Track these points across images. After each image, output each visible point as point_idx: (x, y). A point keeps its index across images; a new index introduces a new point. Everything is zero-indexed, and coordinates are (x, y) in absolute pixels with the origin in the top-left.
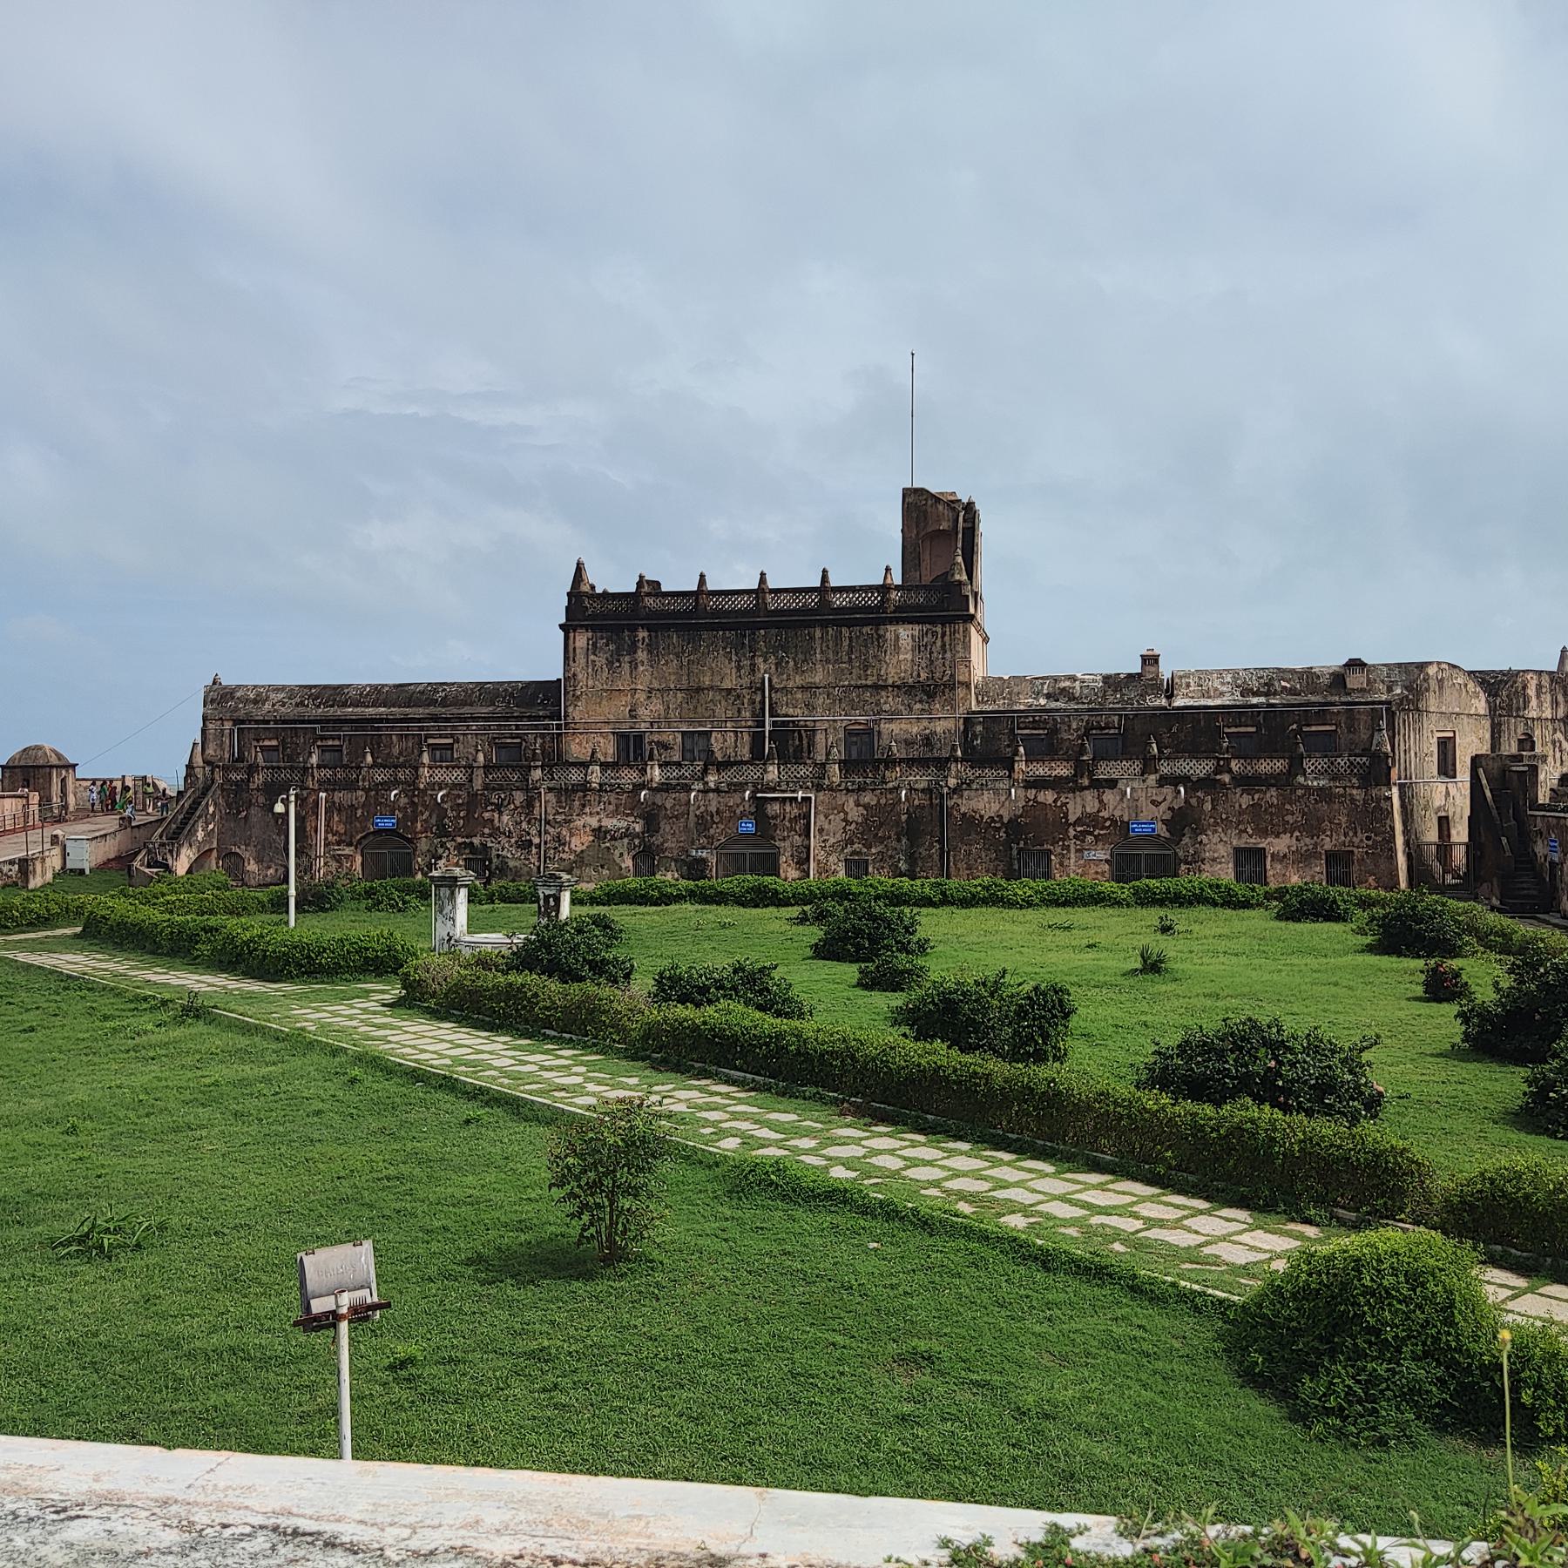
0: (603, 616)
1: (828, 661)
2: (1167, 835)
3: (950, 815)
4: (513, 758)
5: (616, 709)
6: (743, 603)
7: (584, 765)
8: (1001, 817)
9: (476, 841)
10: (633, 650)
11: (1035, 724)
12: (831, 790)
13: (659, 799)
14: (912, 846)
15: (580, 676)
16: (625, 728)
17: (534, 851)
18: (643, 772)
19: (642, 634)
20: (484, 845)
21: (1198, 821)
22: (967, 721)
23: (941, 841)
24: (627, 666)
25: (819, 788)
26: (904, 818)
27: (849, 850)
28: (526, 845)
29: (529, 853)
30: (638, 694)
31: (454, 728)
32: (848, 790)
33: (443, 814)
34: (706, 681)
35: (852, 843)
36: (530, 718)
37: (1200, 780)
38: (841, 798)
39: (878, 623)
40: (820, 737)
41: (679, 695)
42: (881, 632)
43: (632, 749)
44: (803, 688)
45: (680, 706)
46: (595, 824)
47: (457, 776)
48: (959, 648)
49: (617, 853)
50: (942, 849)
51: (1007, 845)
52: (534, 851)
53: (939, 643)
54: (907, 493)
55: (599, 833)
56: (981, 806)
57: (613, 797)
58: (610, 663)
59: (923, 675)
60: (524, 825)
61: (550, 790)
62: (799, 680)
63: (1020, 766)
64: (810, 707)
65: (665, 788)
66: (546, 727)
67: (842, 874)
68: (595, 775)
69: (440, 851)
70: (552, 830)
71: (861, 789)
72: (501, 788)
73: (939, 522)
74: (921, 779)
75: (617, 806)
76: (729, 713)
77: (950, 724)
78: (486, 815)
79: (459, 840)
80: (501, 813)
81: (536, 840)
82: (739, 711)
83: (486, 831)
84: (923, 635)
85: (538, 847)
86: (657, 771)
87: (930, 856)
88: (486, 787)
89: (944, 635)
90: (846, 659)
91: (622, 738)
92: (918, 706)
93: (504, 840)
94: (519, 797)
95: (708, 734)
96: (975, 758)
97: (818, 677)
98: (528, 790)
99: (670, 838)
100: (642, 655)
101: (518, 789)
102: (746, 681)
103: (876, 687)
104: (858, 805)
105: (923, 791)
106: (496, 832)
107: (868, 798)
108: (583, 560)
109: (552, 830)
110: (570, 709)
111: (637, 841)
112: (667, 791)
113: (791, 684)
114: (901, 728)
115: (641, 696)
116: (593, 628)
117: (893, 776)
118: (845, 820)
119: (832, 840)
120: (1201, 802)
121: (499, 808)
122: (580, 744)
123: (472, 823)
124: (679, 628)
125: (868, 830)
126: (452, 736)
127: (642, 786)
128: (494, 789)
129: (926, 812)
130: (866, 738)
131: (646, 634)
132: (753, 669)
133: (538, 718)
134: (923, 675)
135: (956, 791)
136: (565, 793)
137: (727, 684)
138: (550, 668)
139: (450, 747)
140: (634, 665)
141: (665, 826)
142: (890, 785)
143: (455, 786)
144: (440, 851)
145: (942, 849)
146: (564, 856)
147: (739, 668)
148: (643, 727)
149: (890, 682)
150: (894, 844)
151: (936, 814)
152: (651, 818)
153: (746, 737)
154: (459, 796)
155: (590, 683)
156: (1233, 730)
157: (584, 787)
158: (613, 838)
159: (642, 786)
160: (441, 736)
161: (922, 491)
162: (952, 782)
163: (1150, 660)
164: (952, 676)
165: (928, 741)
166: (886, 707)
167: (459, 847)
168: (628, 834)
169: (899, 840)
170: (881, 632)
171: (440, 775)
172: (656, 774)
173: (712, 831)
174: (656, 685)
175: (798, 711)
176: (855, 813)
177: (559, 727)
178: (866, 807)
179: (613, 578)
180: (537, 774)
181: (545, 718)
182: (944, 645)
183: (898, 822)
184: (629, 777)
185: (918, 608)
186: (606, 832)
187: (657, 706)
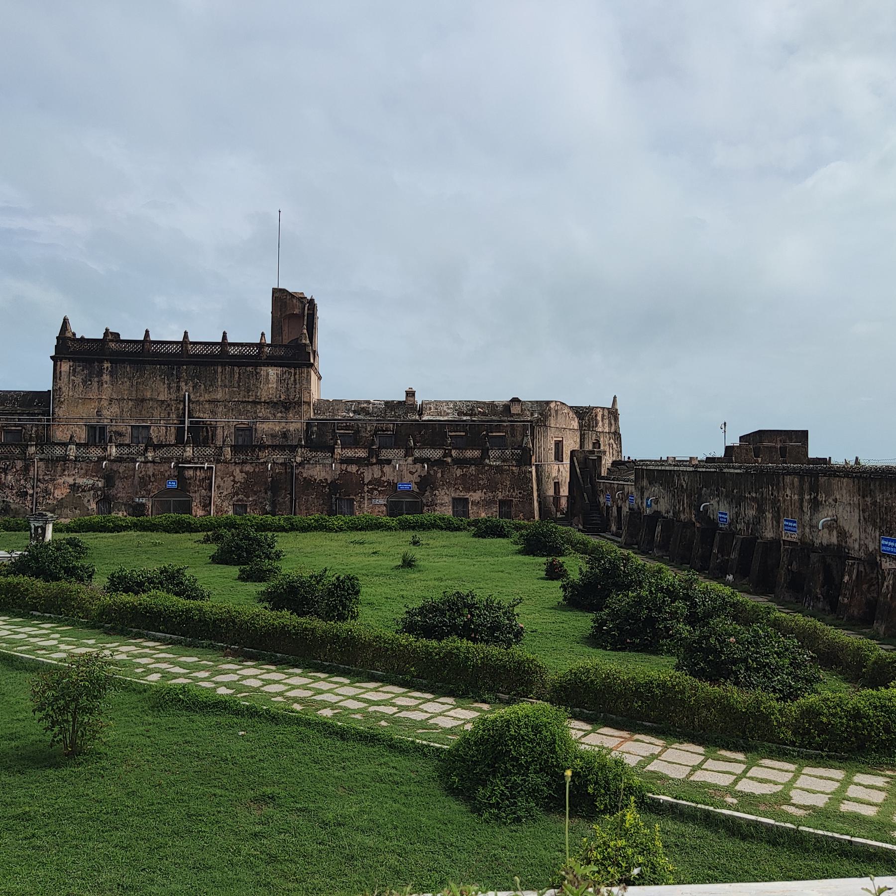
1: (225, 386)
5: (87, 411)
6: (173, 349)
7: (65, 445)
10: (100, 374)
11: (347, 428)
13: (115, 466)
15: (64, 389)
16: (93, 422)
17: (29, 498)
18: (105, 449)
23: (291, 494)
24: (96, 384)
25: (218, 461)
26: (269, 480)
27: (235, 498)
30: (104, 401)
32: (236, 463)
36: (28, 414)
37: (435, 460)
38: (231, 468)
39: (256, 365)
40: (219, 431)
41: (130, 403)
43: (98, 435)
45: (131, 409)
49: (86, 500)
50: (292, 498)
53: (292, 379)
54: (275, 291)
55: (74, 487)
56: (315, 473)
57: (84, 465)
58: (84, 382)
59: (283, 397)
60: (22, 482)
61: (41, 460)
63: (338, 451)
65: (119, 460)
67: (231, 513)
68: (72, 451)
71: (244, 462)
72: (7, 458)
73: (293, 309)
74: (280, 457)
77: (299, 426)
80: (6, 474)
81: (31, 492)
84: (284, 373)
85: (32, 495)
86: (114, 450)
91: (91, 429)
92: (280, 415)
93: (7, 491)
94: (19, 464)
96: (312, 446)
97: (219, 396)
98: (25, 460)
99: (121, 490)
100: (106, 377)
101: (19, 459)
102: (173, 396)
104: (241, 472)
105: (281, 464)
107: (248, 468)
109: (41, 485)
110: (56, 410)
111: (99, 493)
112: (120, 462)
113: (202, 399)
114: (268, 426)
115: (105, 403)
117: (263, 455)
118: (234, 481)
119: (225, 493)
120: (436, 472)
122: (62, 431)
127: (104, 459)
130: (247, 433)
131: (109, 365)
132: (178, 389)
133: (34, 414)
134: (283, 397)
135: (300, 464)
136: (51, 462)
137: (161, 398)
138: (45, 384)
140: (101, 383)
141: (119, 484)
142: (262, 460)
147: (169, 388)
148: (106, 422)
149: (263, 400)
152: (109, 479)
153: (173, 429)
155: (71, 394)
158: (83, 491)
162: (299, 459)
163: (410, 394)
165: (285, 435)
166: (260, 415)
168: (93, 488)
169: (266, 493)
170: (258, 371)
173: (149, 487)
174: (115, 396)
176: (240, 477)
177: (48, 420)
178: (247, 473)
179: (88, 328)
180: (32, 450)
182: (295, 380)
184: (95, 453)
186: (79, 487)
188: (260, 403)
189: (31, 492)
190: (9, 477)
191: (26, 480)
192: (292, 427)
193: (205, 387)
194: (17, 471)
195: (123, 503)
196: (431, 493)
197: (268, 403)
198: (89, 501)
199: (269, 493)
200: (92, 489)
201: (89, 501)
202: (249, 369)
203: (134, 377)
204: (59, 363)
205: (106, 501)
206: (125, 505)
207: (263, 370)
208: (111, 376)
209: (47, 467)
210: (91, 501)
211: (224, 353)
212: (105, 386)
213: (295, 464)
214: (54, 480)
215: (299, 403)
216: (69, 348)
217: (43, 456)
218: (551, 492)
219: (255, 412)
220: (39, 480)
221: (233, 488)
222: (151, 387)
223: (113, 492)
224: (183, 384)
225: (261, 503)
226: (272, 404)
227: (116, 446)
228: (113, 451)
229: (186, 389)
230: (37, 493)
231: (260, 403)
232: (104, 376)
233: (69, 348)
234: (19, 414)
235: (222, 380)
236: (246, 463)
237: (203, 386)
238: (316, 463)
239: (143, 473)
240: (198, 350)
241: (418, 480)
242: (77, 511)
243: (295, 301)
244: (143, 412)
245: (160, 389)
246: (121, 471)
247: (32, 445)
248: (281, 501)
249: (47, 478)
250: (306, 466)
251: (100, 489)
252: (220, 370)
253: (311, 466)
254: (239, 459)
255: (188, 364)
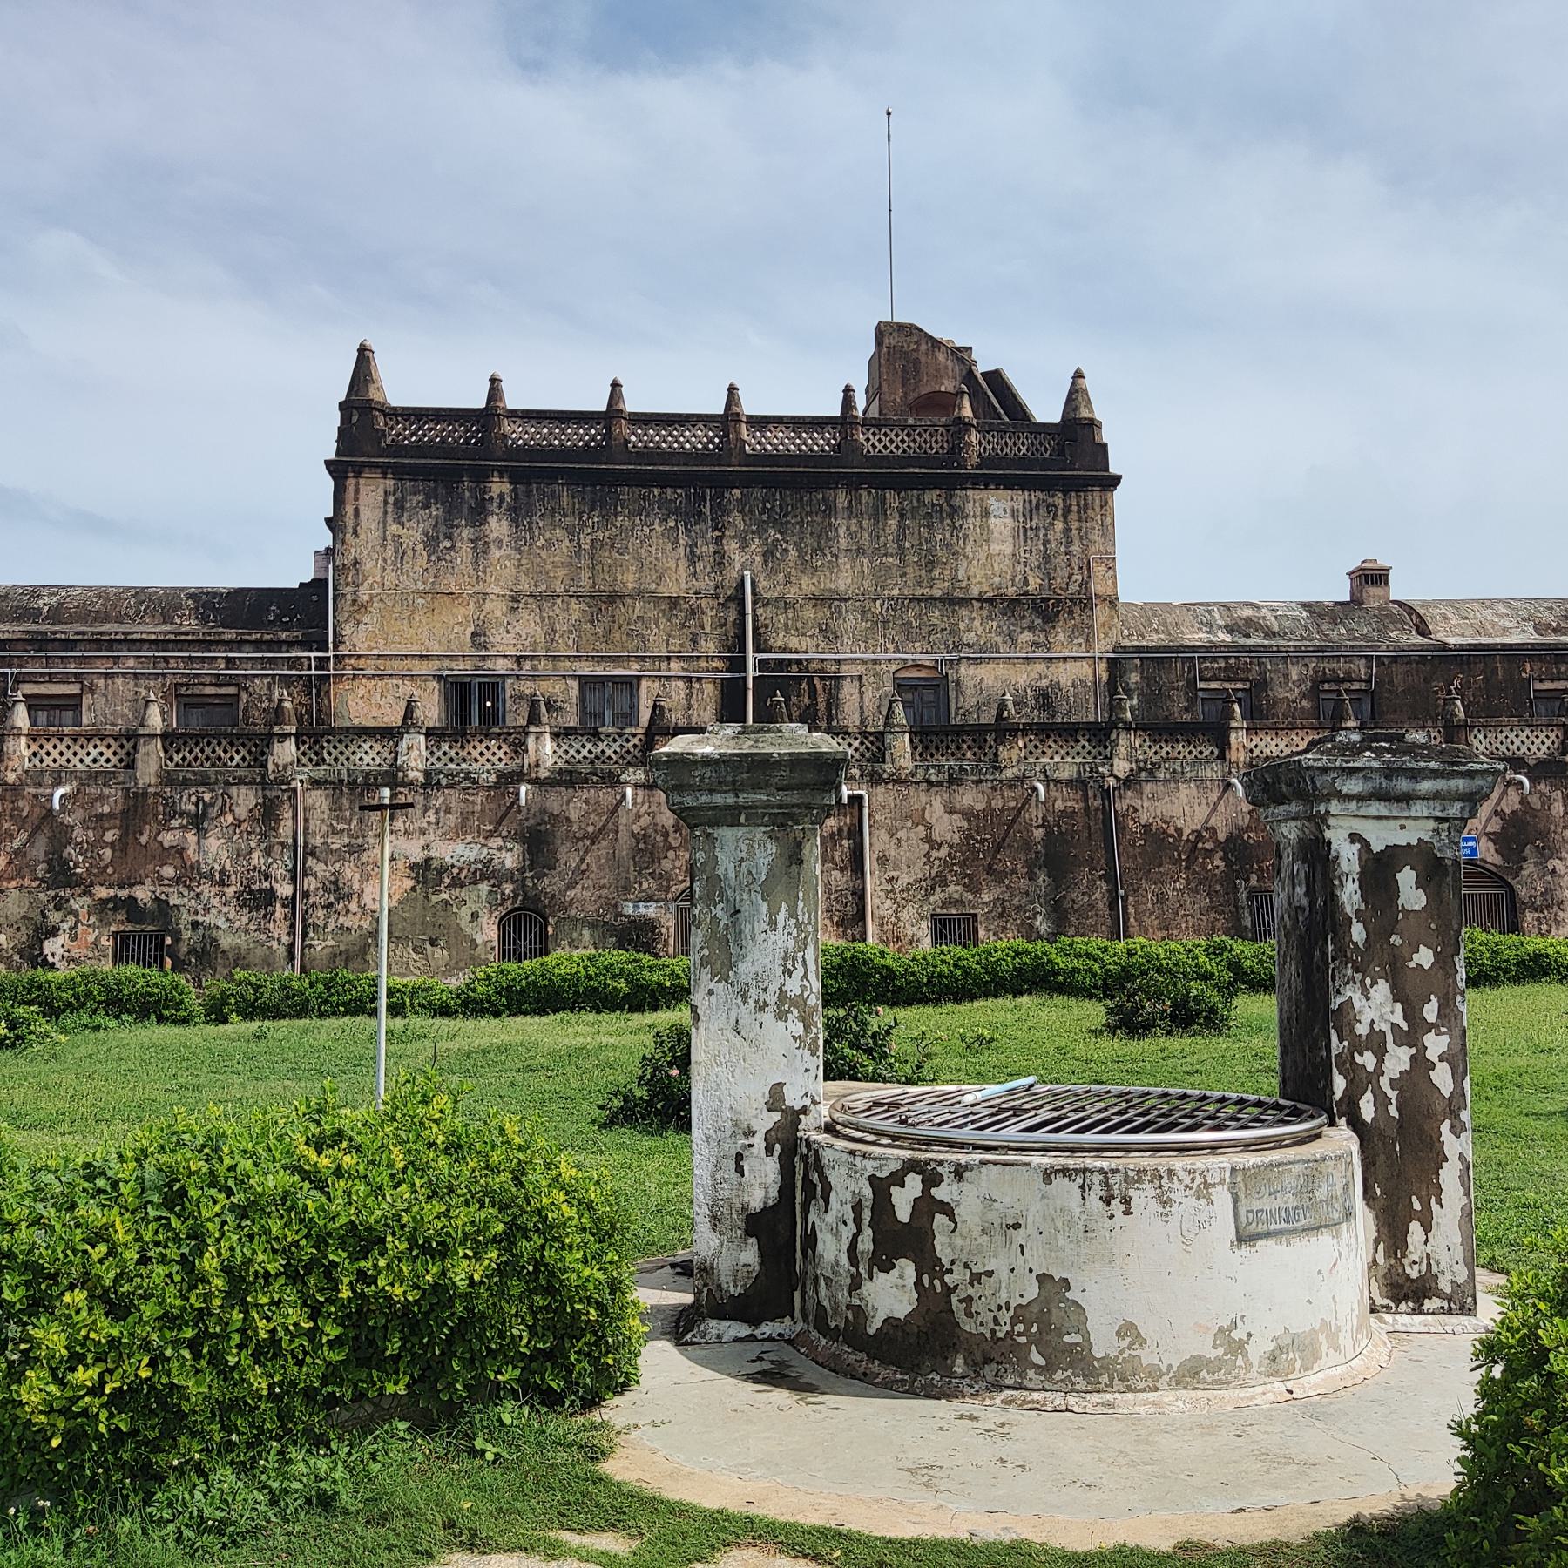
0: (419, 450)
1: (860, 551)
2: (1497, 860)
3: (1122, 828)
4: (216, 727)
5: (442, 634)
6: (695, 439)
7: (388, 734)
8: (1213, 830)
9: (143, 894)
10: (479, 513)
11: (1230, 674)
12: (898, 781)
13: (555, 801)
14: (1056, 889)
15: (368, 565)
16: (462, 669)
17: (279, 912)
18: (519, 748)
19: (499, 487)
20: (161, 904)
21: (1544, 835)
22: (1115, 665)
23: (1110, 878)
24: (465, 550)
25: (876, 779)
26: (1038, 834)
27: (938, 896)
28: (258, 900)
29: (268, 916)
30: (485, 600)
31: (84, 661)
32: (930, 783)
33: (61, 836)
34: (628, 580)
35: (945, 884)
36: (258, 645)
37: (1540, 763)
38: (919, 798)
39: (952, 484)
40: (848, 690)
41: (574, 605)
42: (957, 502)
43: (473, 705)
44: (818, 600)
45: (577, 626)
46: (417, 855)
47: (100, 755)
48: (1095, 535)
49: (465, 913)
50: (1113, 891)
51: (1229, 879)
52: (279, 912)
53: (1059, 526)
54: (881, 332)
55: (426, 873)
56: (1176, 810)
57: (454, 798)
58: (431, 541)
59: (1034, 582)
60: (257, 859)
61: (316, 783)
62: (807, 585)
63: (1238, 739)
64: (829, 634)
65: (567, 779)
66: (294, 663)
67: (926, 945)
68: (416, 755)
69: (55, 917)
70: (319, 868)
71: (954, 780)
72: (203, 781)
73: (938, 378)
74: (1065, 763)
75: (465, 817)
76: (676, 644)
77: (1084, 670)
78: (168, 838)
79: (102, 892)
80: (201, 833)
81: (285, 890)
82: (694, 640)
83: (168, 871)
84: (1031, 511)
85: (291, 903)
86: (548, 746)
87: (1092, 907)
88: (168, 779)
89: (1067, 511)
90: (893, 547)
91: (458, 692)
92: (1026, 637)
93: (208, 891)
94: (245, 800)
95: (631, 684)
96: (1160, 729)
97: (844, 579)
98: (264, 784)
99: (581, 885)
100: (497, 526)
101: (241, 782)
102: (706, 583)
103: (953, 602)
104: (951, 811)
105: (1070, 783)
106: (189, 875)
107: (969, 798)
108: (370, 343)
109: (319, 868)
110: (347, 630)
111: (508, 888)
112: (570, 784)
113: (792, 591)
114: (993, 678)
115: (496, 608)
116: (400, 472)
117: (1012, 754)
118: (928, 840)
119: (905, 879)
120: (1546, 801)
121: (198, 822)
122: (367, 698)
123: (132, 856)
124: (576, 479)
125: (982, 851)
126: (78, 678)
127: (517, 776)
128: (185, 783)
129: (1080, 820)
130: (929, 696)
131: (507, 487)
132: (720, 560)
133: (277, 645)
134: (1034, 582)
135: (1129, 782)
136: (354, 791)
137: (669, 589)
138: (287, 565)
139: (74, 704)
140: (481, 547)
141: (568, 857)
142: (1009, 773)
143: (93, 776)
144: (55, 917)
145: (1113, 891)
146: (347, 921)
147: (692, 558)
148: (501, 667)
149: (975, 592)
150: (1024, 884)
151: (1097, 827)
152: (538, 843)
153: (709, 688)
154: (101, 798)
155: (390, 578)
156: (1548, 685)
157: (392, 776)
158: (457, 883)
159: (517, 776)
160: (51, 679)
161: (909, 330)
162: (1122, 767)
163: (1370, 577)
164: (1085, 584)
165: (1045, 698)
166: (970, 637)
167: (102, 907)
168: (484, 872)
169: (1032, 877)
170: (957, 502)
171: (55, 754)
172: (545, 752)
173: (666, 865)
174: (526, 586)
175: (807, 642)
176: (946, 827)
177: (322, 663)
178: (968, 814)
179: (429, 376)
180: (286, 751)
181: (291, 644)
182: (1067, 531)
183: (1028, 844)
184: (488, 758)
185: (1021, 462)
186: (440, 871)
187: (528, 628)
188: (966, 601)
189: (285, 890)
190: (213, 844)
191: (268, 852)
192: (1066, 675)
193: (801, 556)
194: (238, 823)
195: (584, 921)
196: (1541, 864)
197: (990, 601)
198: (475, 916)
199: (1042, 877)
200: (484, 877)
201: (475, 916)
202: (931, 496)
203: (582, 525)
204: (351, 482)
205: (528, 923)
206: (593, 926)
207: (973, 499)
208: (515, 522)
209: (336, 808)
210: (484, 917)
211: (845, 449)
212: (496, 553)
213: (1112, 782)
214: (361, 849)
215: (1085, 601)
216: (379, 445)
217: (321, 772)
218: (782, 915)
219: (954, 631)
220: (311, 852)
221: (929, 861)
222: (639, 559)
223: (552, 884)
224: (734, 545)
225: (1019, 909)
226: (1006, 606)
227: (555, 736)
228: (545, 752)
229: (743, 560)
230: (306, 895)
231: (966, 601)
232: (493, 521)
233: (379, 445)
234: (229, 645)
235: (850, 534)
236: (960, 782)
237: (793, 553)
238: (1176, 777)
239: (645, 821)
240: (778, 440)
241: (1495, 826)
242: (439, 954)
243: (941, 357)
244: (616, 636)
245: (659, 559)
246: (574, 816)
247: (286, 736)
248: (1081, 900)
249: (336, 842)
250: (1148, 788)
251: (509, 876)
252: (842, 499)
253: (1160, 788)
254: (939, 768)
255: (746, 481)
